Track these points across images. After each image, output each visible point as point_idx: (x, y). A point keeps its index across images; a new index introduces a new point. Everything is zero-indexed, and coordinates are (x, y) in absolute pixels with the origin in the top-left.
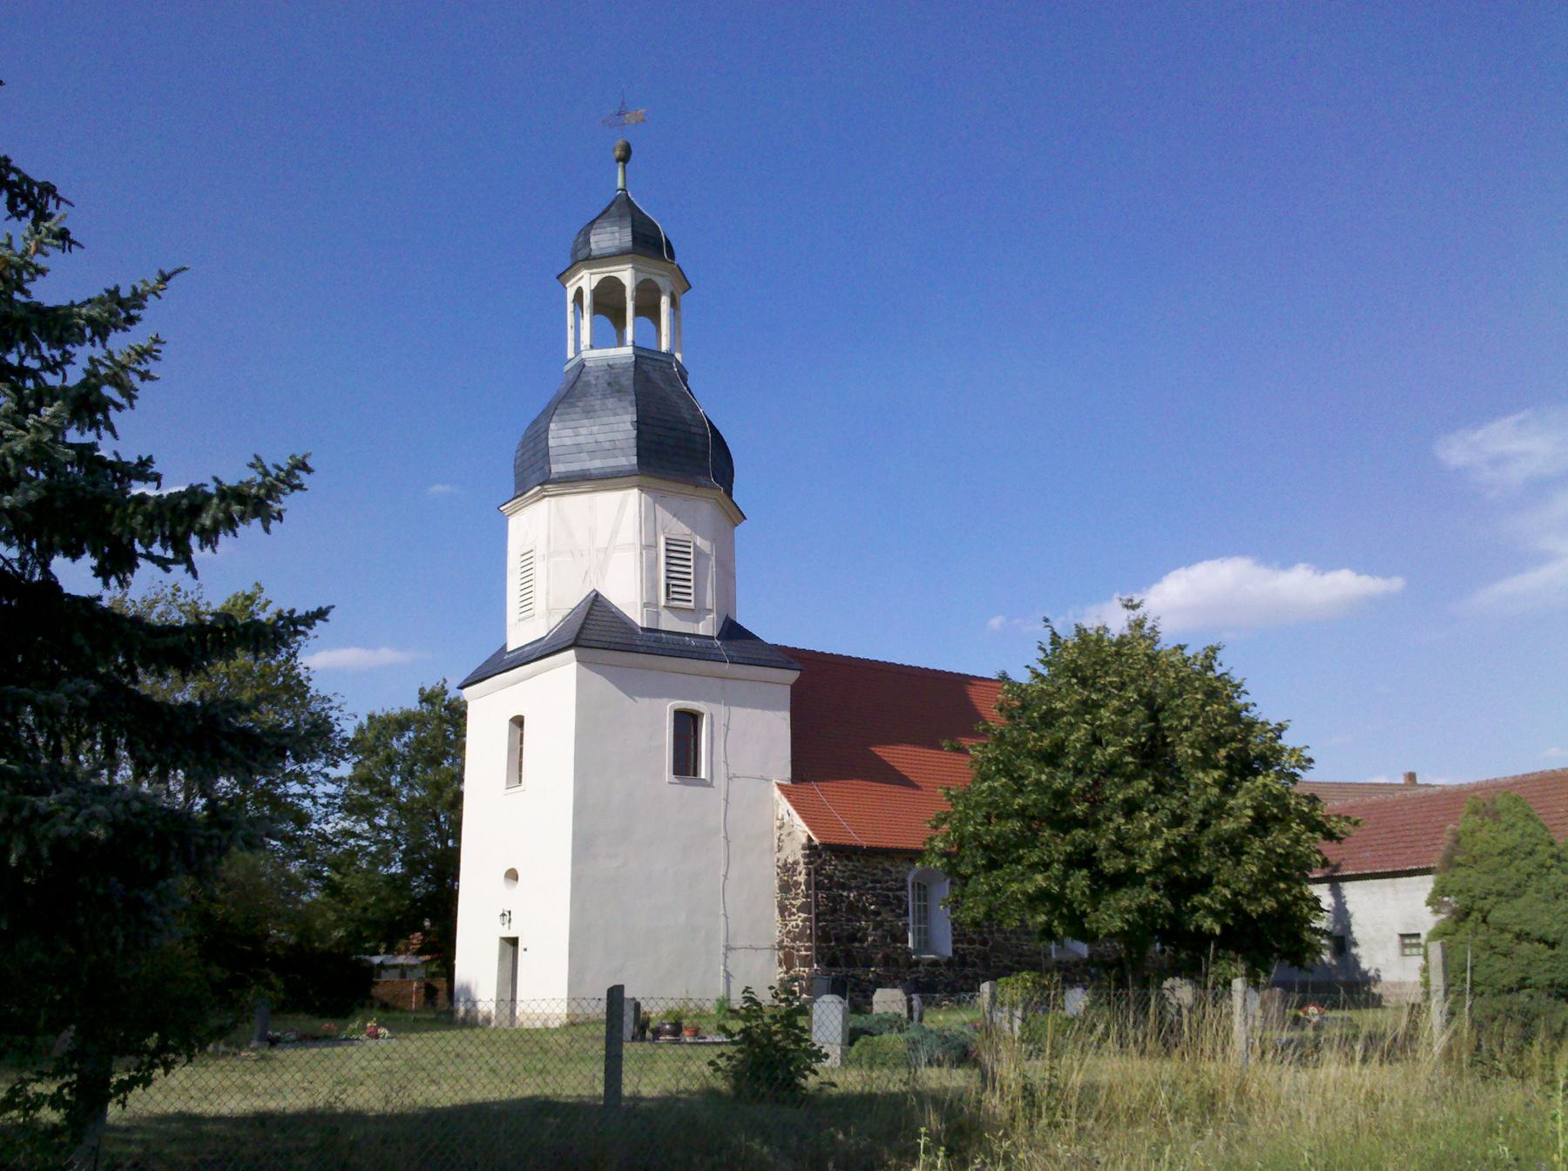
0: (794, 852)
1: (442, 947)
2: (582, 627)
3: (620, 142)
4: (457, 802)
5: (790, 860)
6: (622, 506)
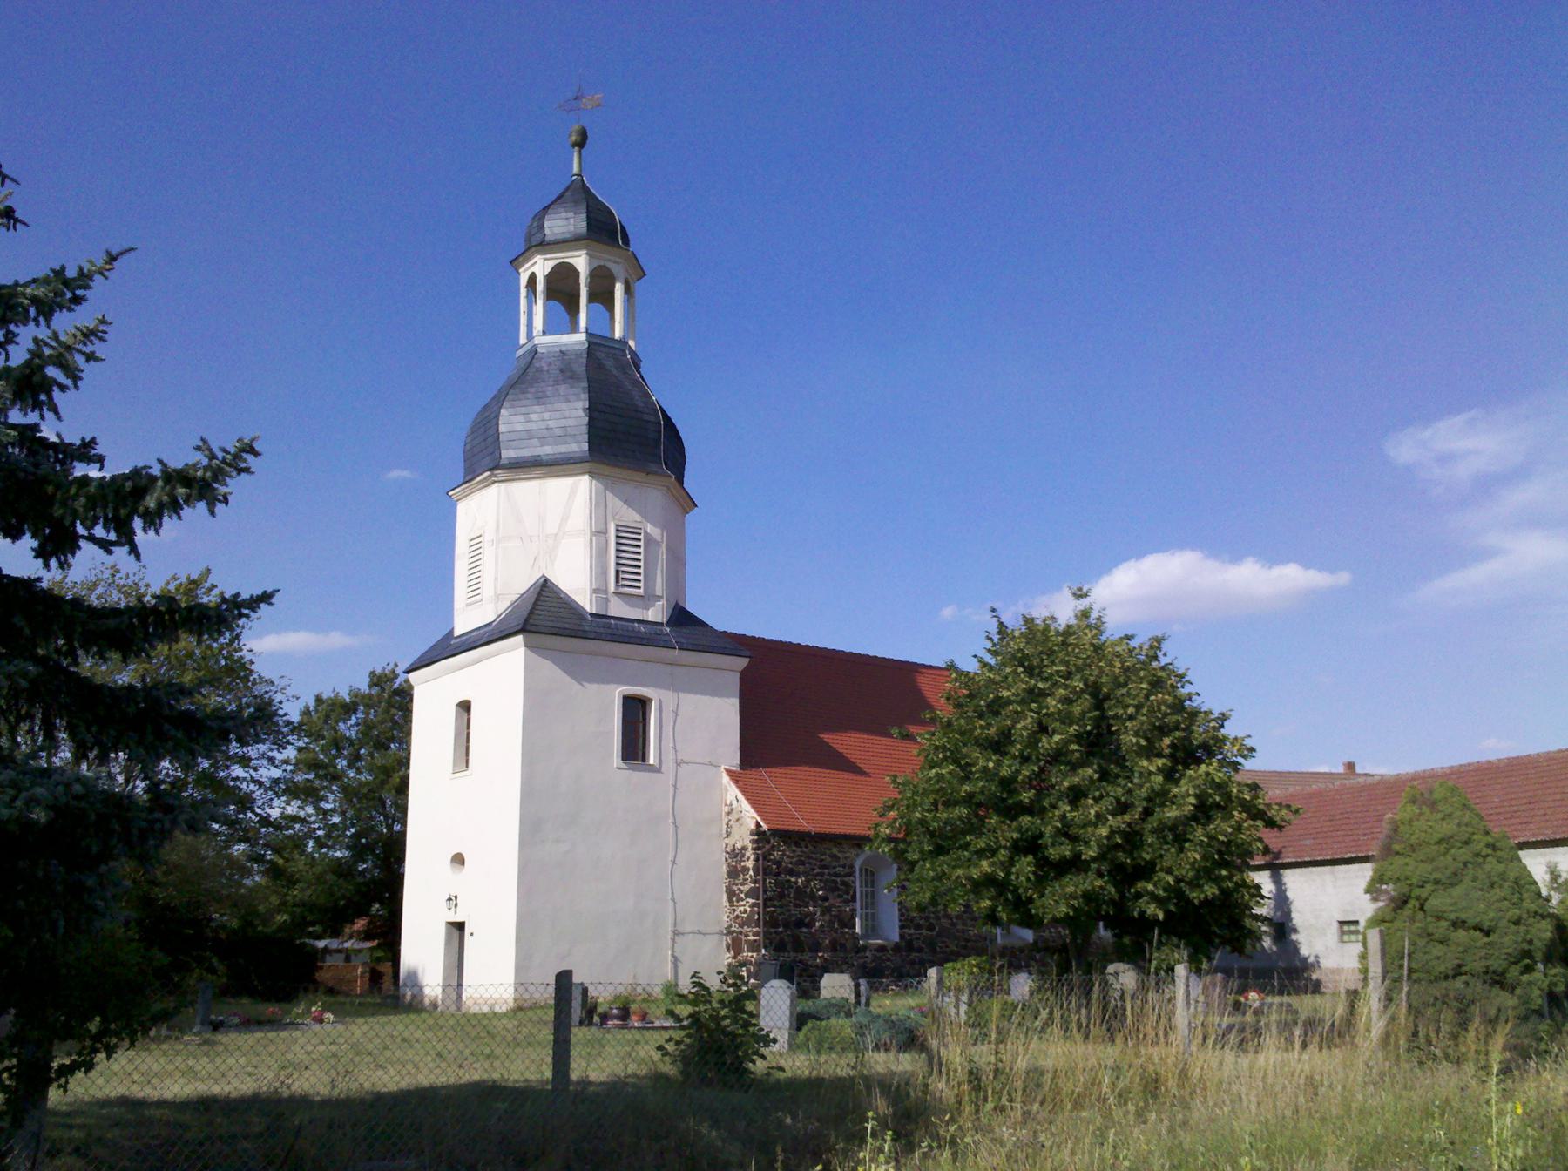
0: (743, 837)
1: (388, 933)
2: (531, 612)
3: (577, 127)
4: (403, 788)
5: (739, 846)
6: (573, 493)
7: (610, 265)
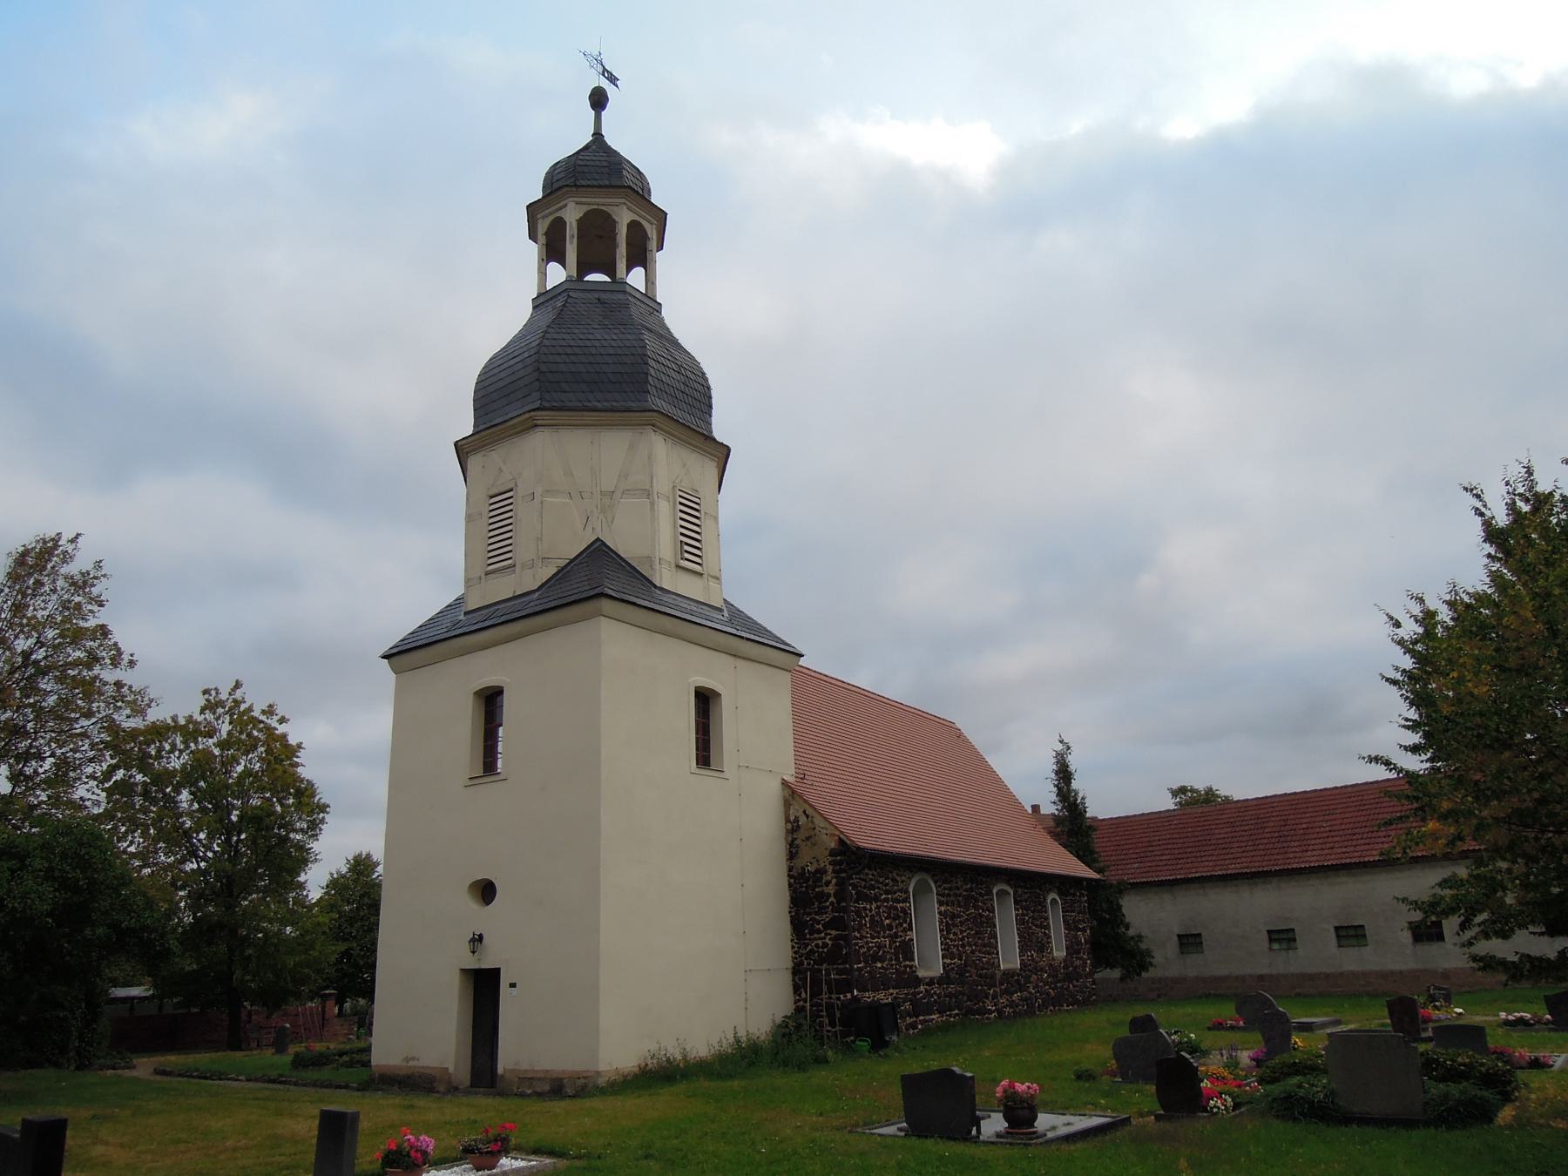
7: (644, 223)
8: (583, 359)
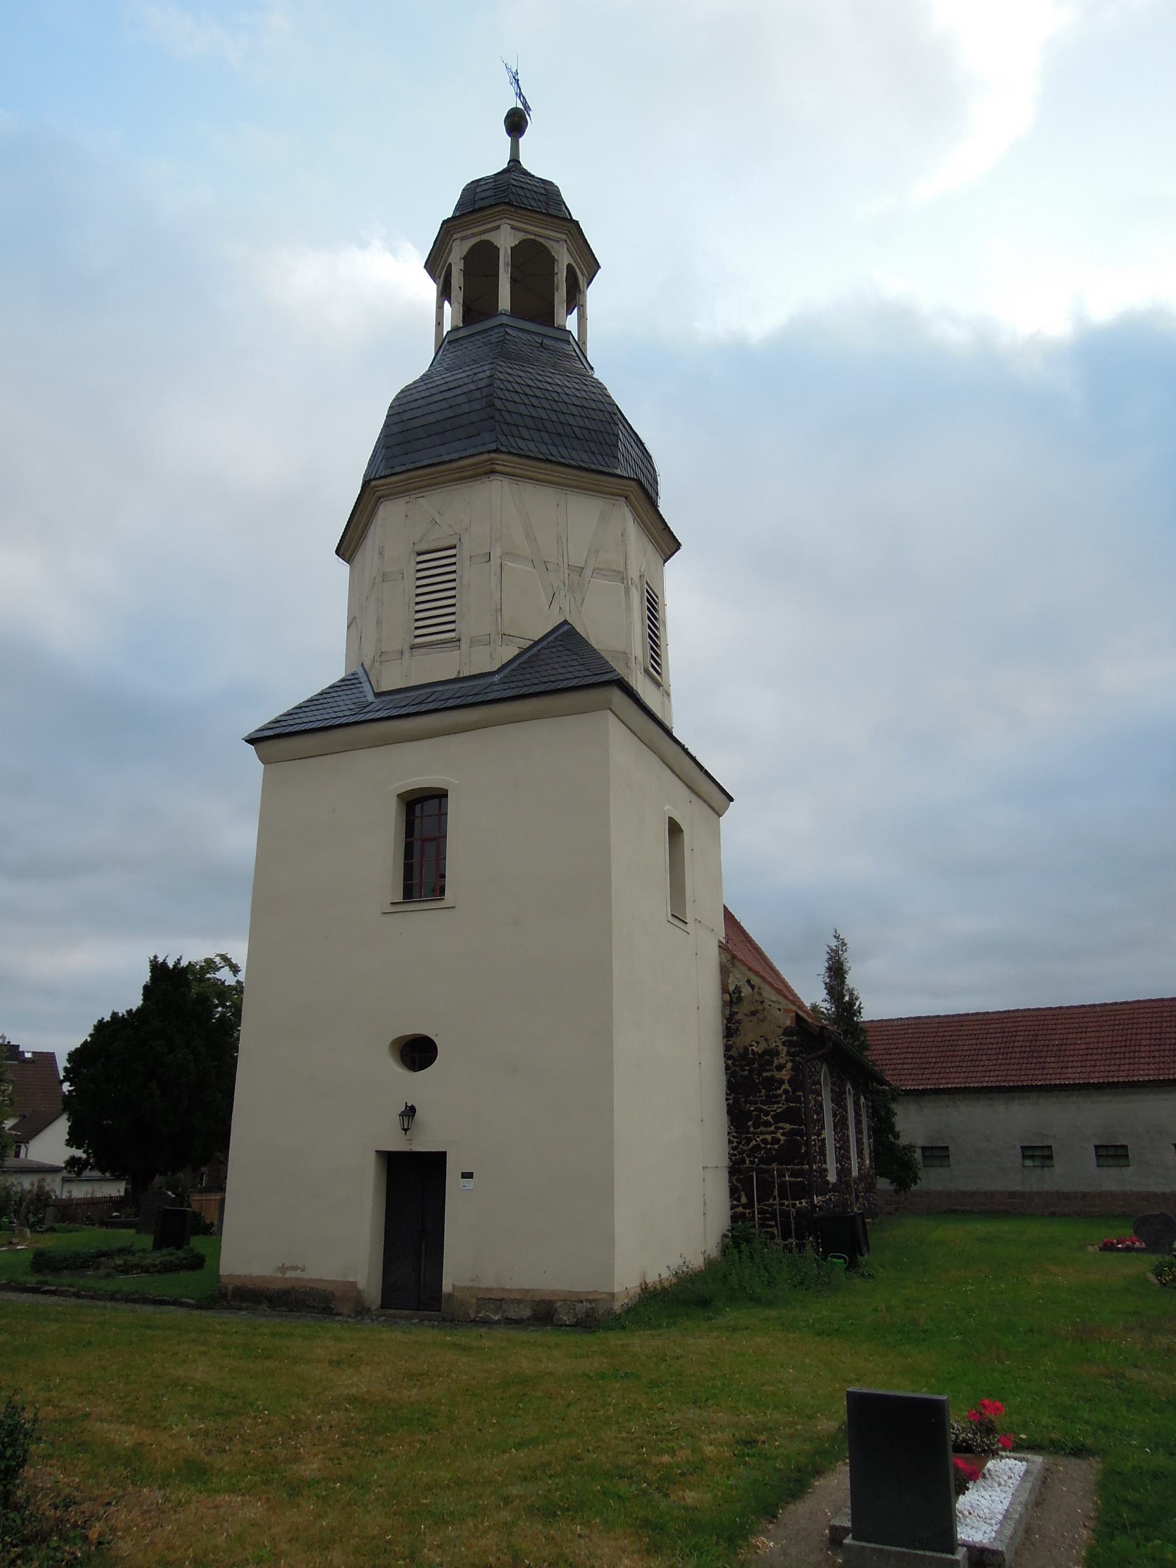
8: (546, 404)
